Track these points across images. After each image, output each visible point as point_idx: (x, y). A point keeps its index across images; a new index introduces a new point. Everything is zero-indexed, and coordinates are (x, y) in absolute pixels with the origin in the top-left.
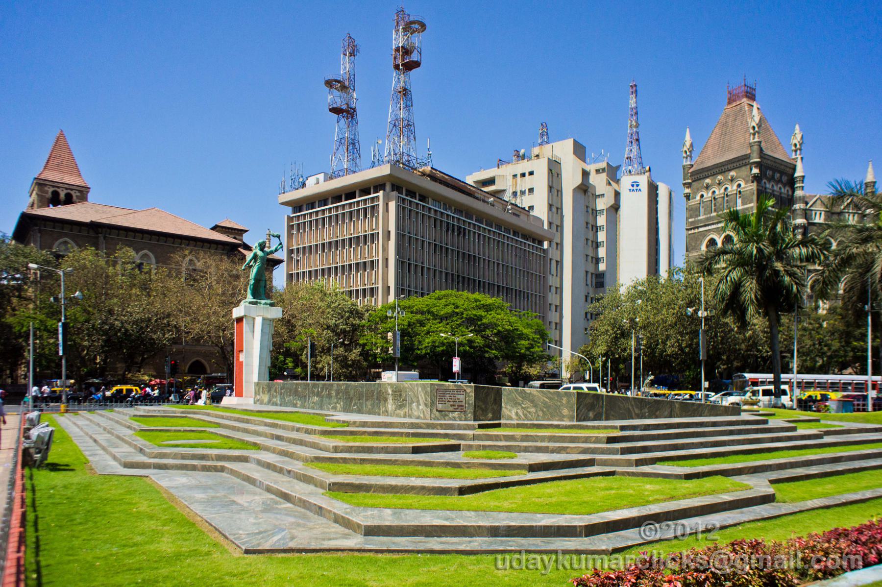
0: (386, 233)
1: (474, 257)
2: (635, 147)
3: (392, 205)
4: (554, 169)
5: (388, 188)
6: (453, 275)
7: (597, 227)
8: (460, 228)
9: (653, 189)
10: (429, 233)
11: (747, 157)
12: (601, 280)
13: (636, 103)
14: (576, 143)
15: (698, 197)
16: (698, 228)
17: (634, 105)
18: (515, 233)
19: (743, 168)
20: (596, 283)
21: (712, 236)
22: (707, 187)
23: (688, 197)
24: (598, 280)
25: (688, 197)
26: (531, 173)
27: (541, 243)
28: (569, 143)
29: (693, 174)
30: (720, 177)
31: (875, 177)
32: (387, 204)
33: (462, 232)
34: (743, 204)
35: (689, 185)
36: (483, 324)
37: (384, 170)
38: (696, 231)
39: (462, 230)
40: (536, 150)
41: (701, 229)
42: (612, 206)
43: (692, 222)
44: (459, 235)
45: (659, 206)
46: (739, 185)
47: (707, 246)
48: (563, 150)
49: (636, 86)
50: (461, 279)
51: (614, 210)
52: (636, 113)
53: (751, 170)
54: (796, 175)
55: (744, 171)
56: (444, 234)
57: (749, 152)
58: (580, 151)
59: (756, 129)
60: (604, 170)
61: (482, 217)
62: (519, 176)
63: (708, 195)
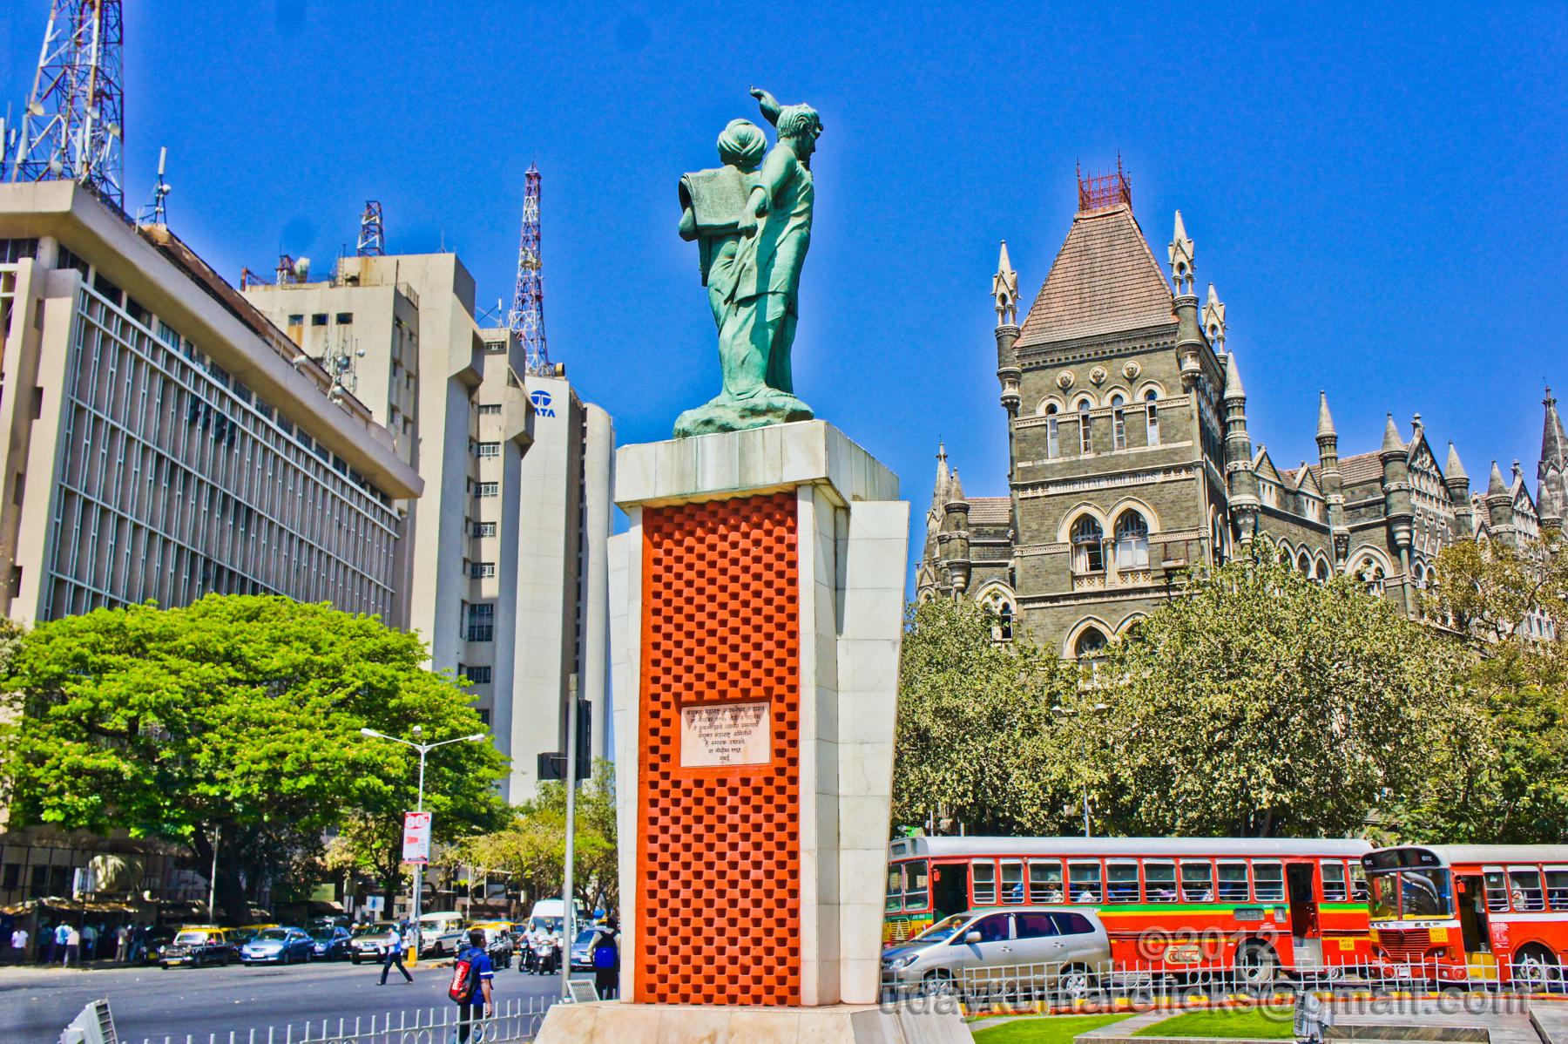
0: (28, 393)
1: (249, 510)
2: (532, 316)
3: (60, 312)
4: (405, 310)
5: (47, 251)
6: (194, 555)
7: (479, 484)
8: (222, 420)
9: (578, 416)
10: (144, 419)
11: (1171, 330)
12: (485, 621)
13: (539, 215)
14: (459, 266)
15: (1041, 411)
16: (1045, 485)
17: (533, 219)
18: (339, 463)
19: (1160, 355)
20: (472, 628)
21: (1084, 509)
22: (1065, 388)
23: (1012, 406)
24: (477, 621)
25: (1012, 406)
26: (345, 319)
27: (386, 499)
28: (443, 265)
29: (1025, 352)
30: (1098, 368)
31: (1335, 428)
32: (40, 304)
33: (225, 432)
34: (1164, 438)
35: (1015, 378)
36: (401, 708)
37: (56, 197)
38: (1040, 492)
39: (202, 409)
40: (350, 265)
41: (1052, 490)
42: (515, 439)
43: (1025, 470)
44: (218, 439)
45: (588, 457)
46: (1151, 395)
47: (1072, 533)
48: (430, 275)
49: (538, 177)
50: (213, 571)
51: (517, 450)
52: (538, 238)
53: (1179, 362)
54: (1227, 395)
55: (1163, 363)
56: (184, 428)
57: (1174, 319)
58: (464, 286)
59: (1010, 302)
60: (502, 346)
61: (274, 401)
62: (308, 320)
63: (1068, 408)
